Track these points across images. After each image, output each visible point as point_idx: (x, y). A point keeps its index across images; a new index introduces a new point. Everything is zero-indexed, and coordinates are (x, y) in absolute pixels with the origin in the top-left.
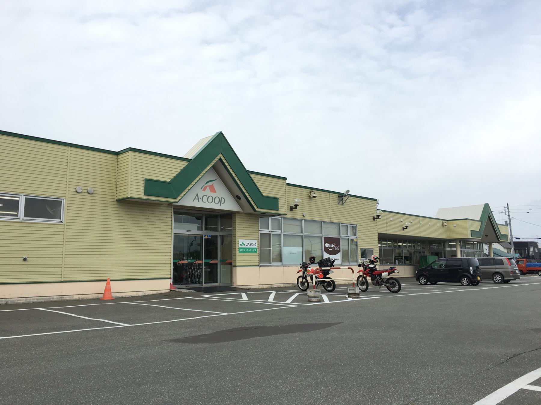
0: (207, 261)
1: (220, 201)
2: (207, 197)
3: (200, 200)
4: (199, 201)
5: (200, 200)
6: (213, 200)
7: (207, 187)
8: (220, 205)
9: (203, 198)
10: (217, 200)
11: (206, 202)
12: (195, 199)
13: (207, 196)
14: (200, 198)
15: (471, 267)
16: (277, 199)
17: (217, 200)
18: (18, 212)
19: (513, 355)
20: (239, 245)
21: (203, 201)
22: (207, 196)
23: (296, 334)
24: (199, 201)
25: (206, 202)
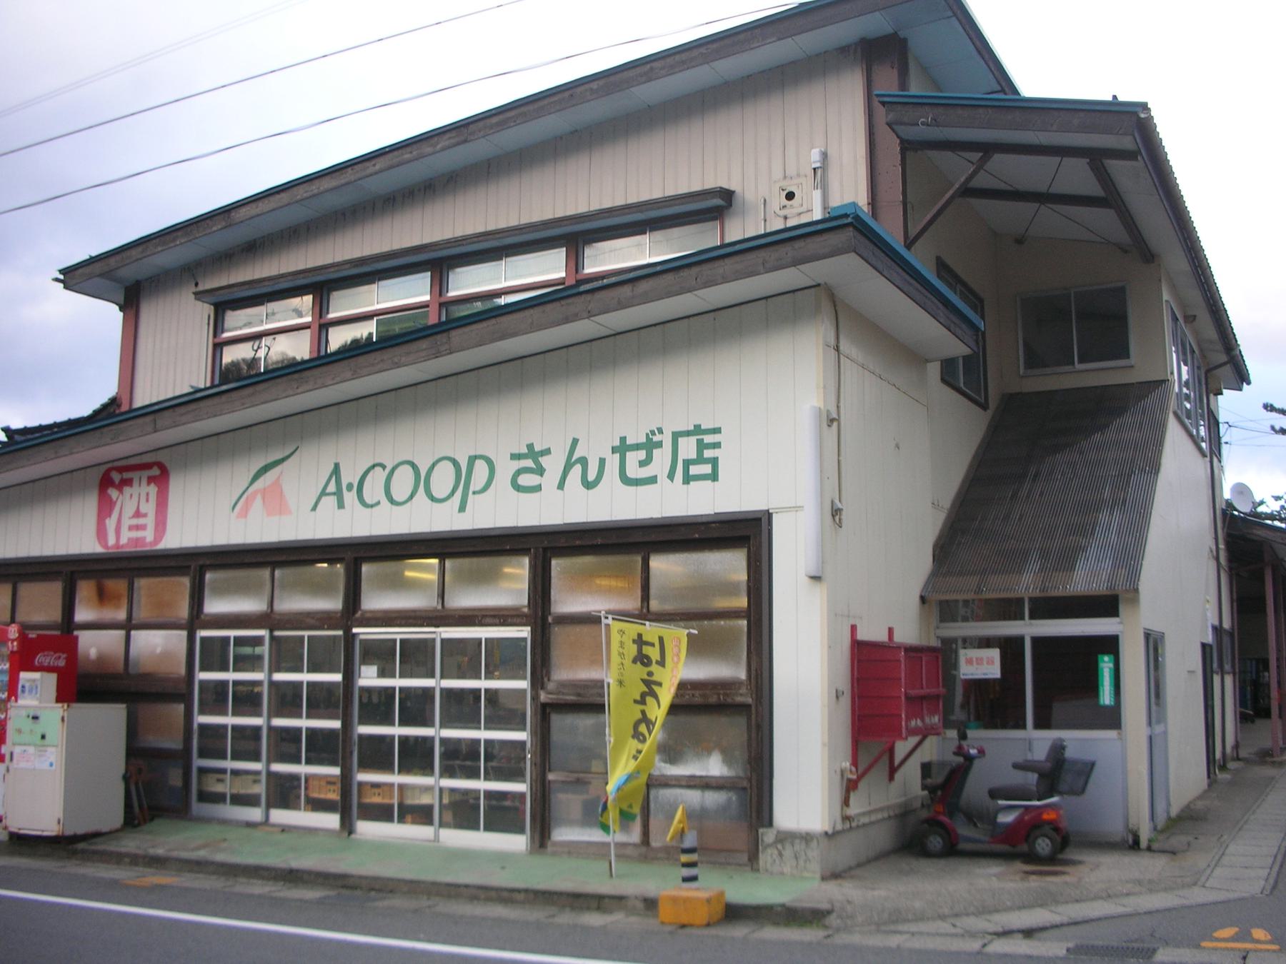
0: (387, 801)
1: (462, 478)
2: (387, 470)
3: (350, 497)
4: (341, 505)
5: (350, 497)
6: (422, 481)
7: (255, 493)
8: (462, 508)
9: (396, 473)
10: (443, 480)
11: (378, 503)
12: (324, 493)
13: (384, 467)
14: (350, 487)
15: (1105, 707)
16: (673, 433)
17: (443, 480)
18: (958, 357)
19: (984, 937)
20: (381, 793)
21: (395, 498)
22: (384, 467)
23: (987, 358)
24: (341, 505)
25: (378, 503)
